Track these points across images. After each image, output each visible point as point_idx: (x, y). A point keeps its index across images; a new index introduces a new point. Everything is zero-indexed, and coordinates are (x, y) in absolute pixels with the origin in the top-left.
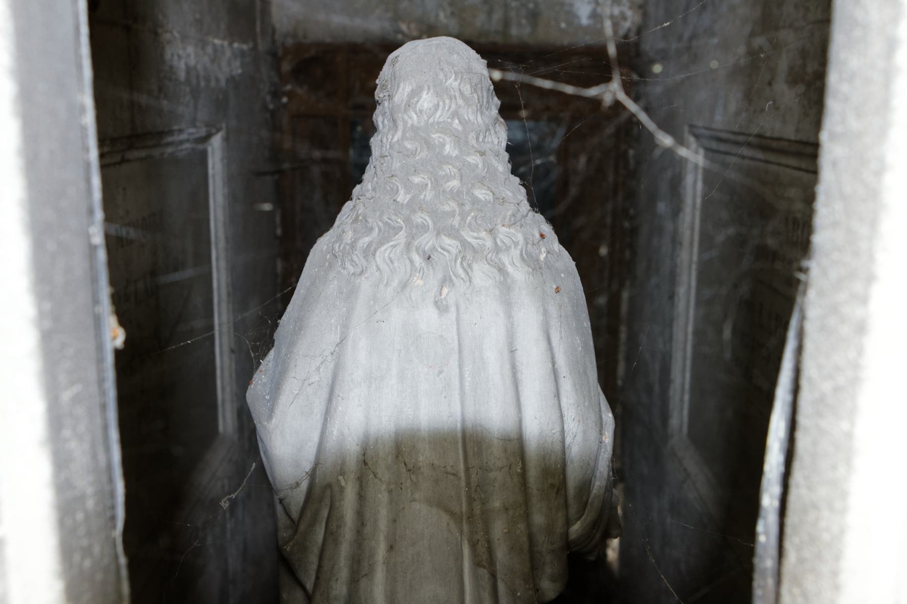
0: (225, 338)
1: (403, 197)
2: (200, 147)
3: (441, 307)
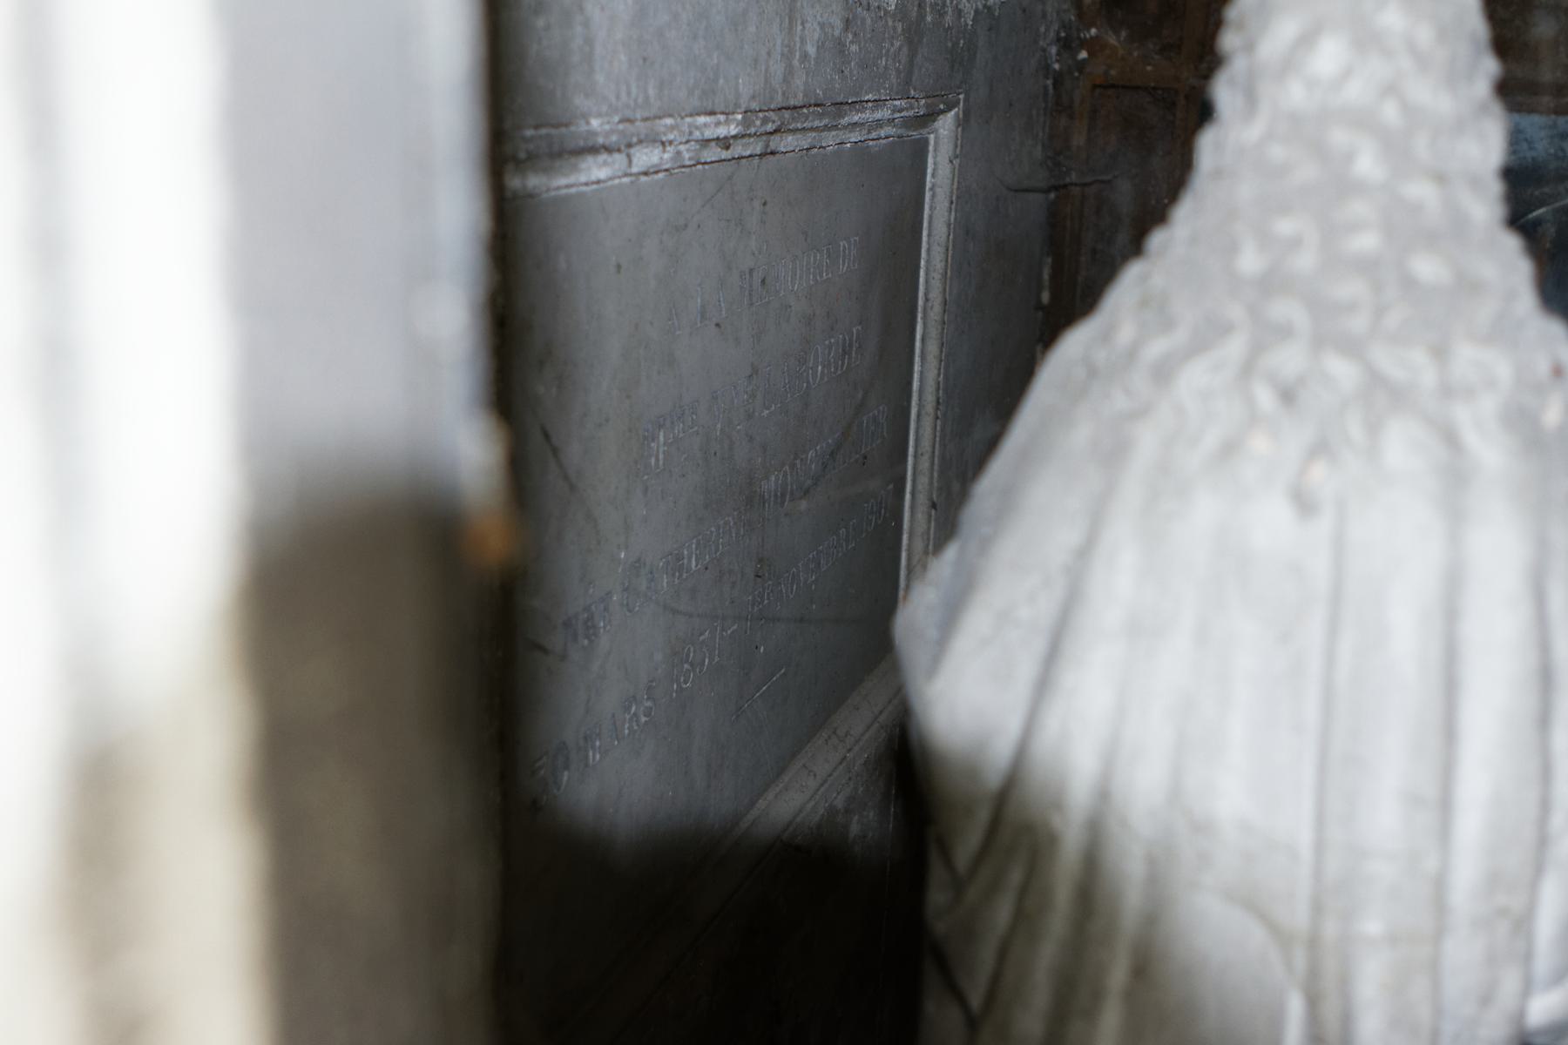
0: (923, 480)
1: (1250, 261)
2: (915, 134)
3: (1304, 503)
